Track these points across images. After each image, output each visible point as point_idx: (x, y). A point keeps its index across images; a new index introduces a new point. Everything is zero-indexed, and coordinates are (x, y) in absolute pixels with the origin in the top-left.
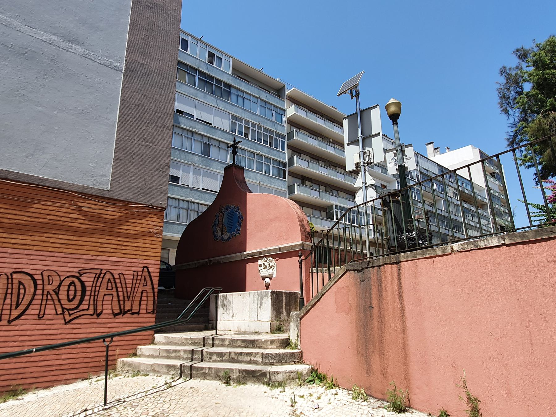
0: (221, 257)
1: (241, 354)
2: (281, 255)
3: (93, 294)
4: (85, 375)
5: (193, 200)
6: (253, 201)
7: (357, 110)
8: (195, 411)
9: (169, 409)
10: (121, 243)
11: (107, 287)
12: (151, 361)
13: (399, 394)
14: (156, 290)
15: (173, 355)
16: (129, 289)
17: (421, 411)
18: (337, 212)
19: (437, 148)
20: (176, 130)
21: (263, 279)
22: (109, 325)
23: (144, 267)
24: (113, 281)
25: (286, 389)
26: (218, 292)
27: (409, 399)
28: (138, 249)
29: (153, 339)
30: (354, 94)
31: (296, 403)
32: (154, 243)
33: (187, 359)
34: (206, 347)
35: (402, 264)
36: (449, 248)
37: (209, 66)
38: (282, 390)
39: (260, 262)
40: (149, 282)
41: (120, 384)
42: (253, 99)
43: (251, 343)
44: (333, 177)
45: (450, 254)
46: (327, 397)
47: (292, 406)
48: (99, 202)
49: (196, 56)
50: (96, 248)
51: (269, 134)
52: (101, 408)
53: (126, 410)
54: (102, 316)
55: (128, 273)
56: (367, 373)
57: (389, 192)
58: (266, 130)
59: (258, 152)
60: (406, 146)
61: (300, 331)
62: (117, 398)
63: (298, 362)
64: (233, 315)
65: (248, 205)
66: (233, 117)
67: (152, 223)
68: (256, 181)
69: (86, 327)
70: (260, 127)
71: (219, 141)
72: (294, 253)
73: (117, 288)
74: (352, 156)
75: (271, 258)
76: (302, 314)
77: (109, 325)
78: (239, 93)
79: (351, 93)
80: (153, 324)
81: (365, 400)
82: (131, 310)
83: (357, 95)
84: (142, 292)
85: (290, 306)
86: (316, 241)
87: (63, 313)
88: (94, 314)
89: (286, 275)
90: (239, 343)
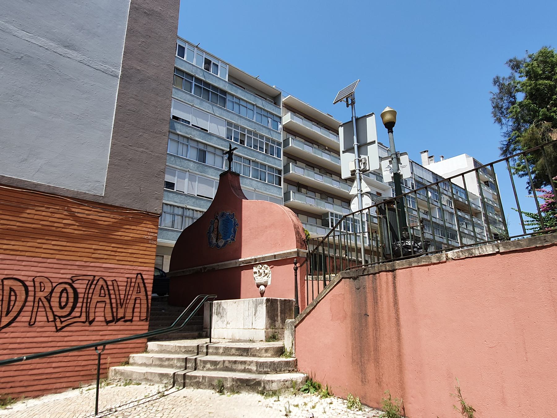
0: (216, 264)
1: (235, 362)
3: (85, 301)
4: (76, 384)
5: (188, 207)
7: (352, 118)
10: (115, 249)
11: (100, 294)
12: (144, 370)
16: (122, 297)
18: (332, 220)
19: (432, 157)
20: (172, 136)
21: (258, 286)
23: (138, 274)
25: (281, 398)
26: (213, 300)
27: (404, 409)
29: (146, 347)
30: (350, 102)
31: (290, 412)
33: (180, 367)
34: (199, 356)
36: (444, 256)
37: (205, 73)
38: (277, 399)
39: (255, 269)
40: (143, 289)
41: (112, 394)
42: (249, 106)
43: (246, 351)
44: (328, 185)
45: (445, 262)
46: (322, 407)
47: (286, 415)
49: (192, 63)
51: (264, 141)
54: (94, 323)
55: (122, 280)
56: (362, 382)
57: (384, 200)
58: (262, 137)
59: (254, 159)
60: (401, 154)
61: (295, 339)
62: (109, 407)
63: (293, 370)
64: (228, 323)
65: (243, 212)
66: (229, 124)
67: (147, 230)
69: (77, 335)
70: (256, 134)
71: (215, 148)
72: (289, 260)
73: (110, 295)
74: (347, 163)
75: (266, 266)
76: (297, 322)
77: (101, 333)
78: (235, 100)
79: (347, 101)
80: (147, 331)
81: (360, 409)
82: (124, 317)
83: (353, 103)
84: (136, 300)
85: (285, 314)
87: (54, 321)
89: (281, 283)
90: (233, 351)
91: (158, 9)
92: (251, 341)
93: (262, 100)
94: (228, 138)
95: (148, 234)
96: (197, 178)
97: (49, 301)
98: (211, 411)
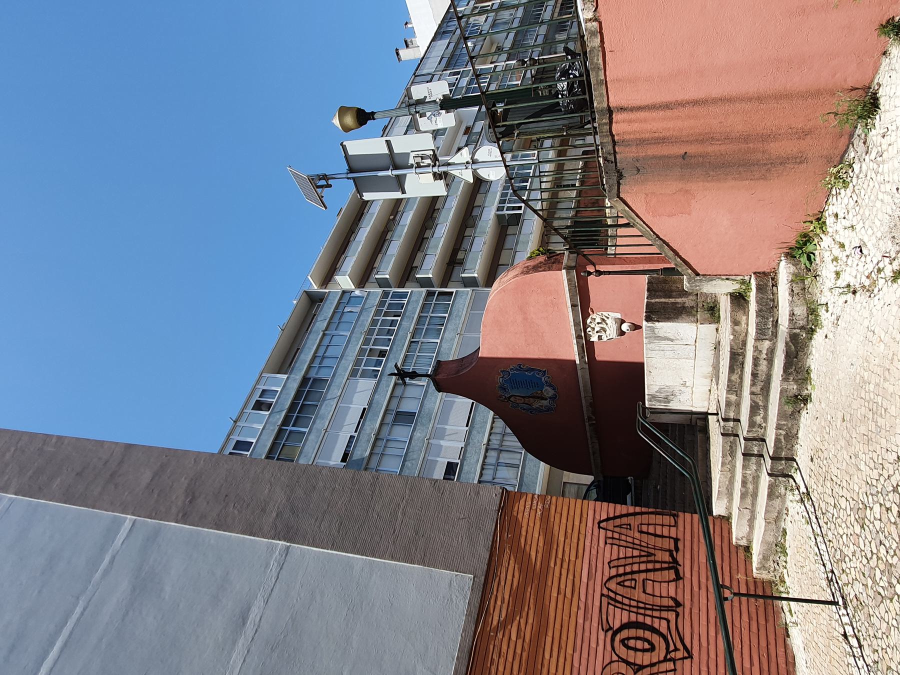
0: (583, 402)
1: (754, 375)
2: (583, 303)
3: (642, 611)
4: (780, 632)
5: (485, 441)
6: (495, 343)
7: (348, 178)
8: (856, 456)
9: (851, 500)
10: (559, 562)
11: (631, 587)
12: (760, 523)
13: (843, 107)
14: (631, 510)
15: (750, 486)
16: (636, 553)
17: (876, 70)
18: (508, 209)
19: (406, 42)
20: (373, 464)
21: (622, 333)
22: (696, 589)
23: (599, 527)
24: (622, 578)
25: (823, 301)
26: (644, 408)
27: (853, 89)
28: (569, 535)
29: (721, 517)
30: (323, 182)
31: (849, 286)
32: (559, 510)
33: (759, 465)
34: (740, 433)
35: (612, 104)
36: (589, 24)
37: (276, 410)
38: (824, 308)
39: (594, 338)
40: (624, 520)
41: (800, 575)
42: (326, 341)
43: (736, 358)
44: (451, 214)
45: (600, 23)
46: (841, 232)
47: (854, 292)
48: (492, 593)
49: (259, 429)
50: (567, 602)
51: (382, 318)
52: (843, 611)
53: (848, 571)
54: (680, 599)
55: (609, 553)
56: (801, 163)
57: (490, 127)
58: (374, 322)
59: (409, 335)
60: (410, 98)
61: (718, 276)
62: (824, 583)
63: (773, 279)
64: (684, 385)
65: (500, 356)
66: (354, 373)
67: (527, 510)
68: (456, 340)
69: (699, 626)
70: (370, 332)
71: (391, 397)
72: (581, 282)
73: (632, 573)
74: (421, 185)
75: (589, 321)
76: (690, 271)
77: (696, 589)
78: (316, 364)
79: (321, 187)
80: (696, 517)
81: (851, 166)
82: (670, 551)
83: (325, 177)
84: (641, 532)
85: (672, 291)
86: (558, 245)
87: (674, 660)
88: (676, 611)
89: (618, 298)
90: (735, 377)
91: (184, 482)
92: (717, 347)
93: (316, 321)
94: (376, 376)
95: (534, 508)
96: (439, 426)
97: (642, 667)
98: (840, 419)
